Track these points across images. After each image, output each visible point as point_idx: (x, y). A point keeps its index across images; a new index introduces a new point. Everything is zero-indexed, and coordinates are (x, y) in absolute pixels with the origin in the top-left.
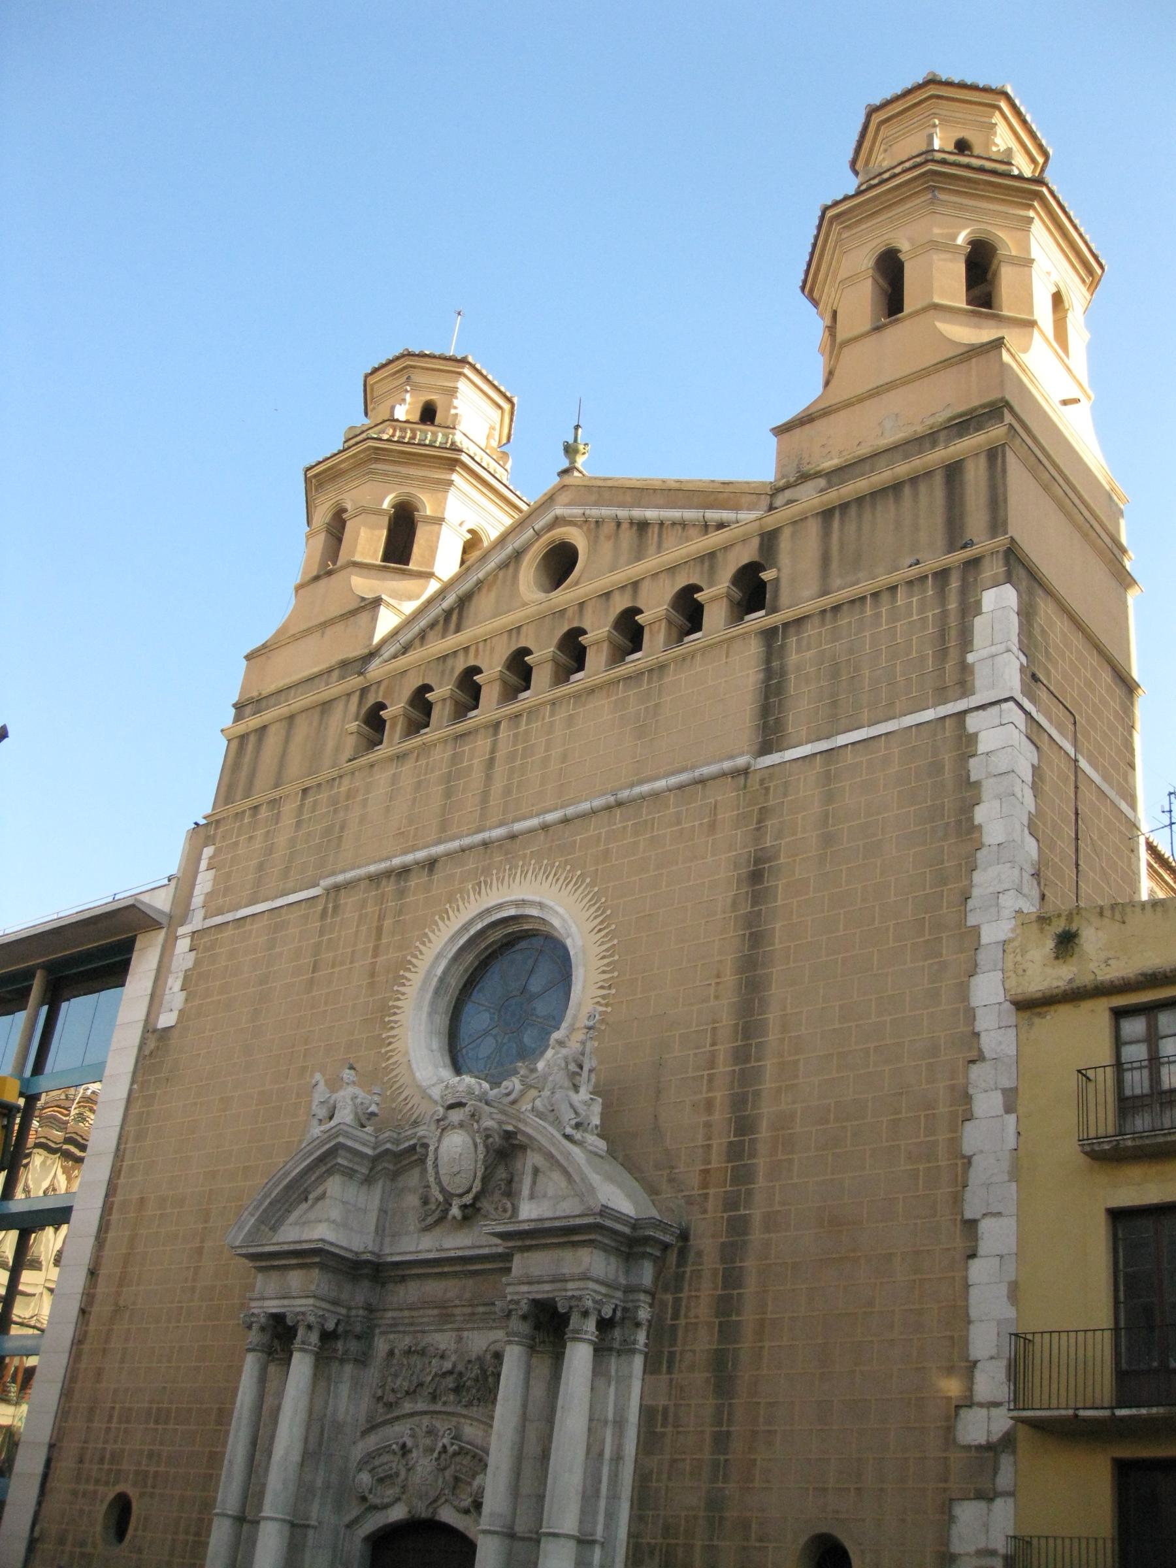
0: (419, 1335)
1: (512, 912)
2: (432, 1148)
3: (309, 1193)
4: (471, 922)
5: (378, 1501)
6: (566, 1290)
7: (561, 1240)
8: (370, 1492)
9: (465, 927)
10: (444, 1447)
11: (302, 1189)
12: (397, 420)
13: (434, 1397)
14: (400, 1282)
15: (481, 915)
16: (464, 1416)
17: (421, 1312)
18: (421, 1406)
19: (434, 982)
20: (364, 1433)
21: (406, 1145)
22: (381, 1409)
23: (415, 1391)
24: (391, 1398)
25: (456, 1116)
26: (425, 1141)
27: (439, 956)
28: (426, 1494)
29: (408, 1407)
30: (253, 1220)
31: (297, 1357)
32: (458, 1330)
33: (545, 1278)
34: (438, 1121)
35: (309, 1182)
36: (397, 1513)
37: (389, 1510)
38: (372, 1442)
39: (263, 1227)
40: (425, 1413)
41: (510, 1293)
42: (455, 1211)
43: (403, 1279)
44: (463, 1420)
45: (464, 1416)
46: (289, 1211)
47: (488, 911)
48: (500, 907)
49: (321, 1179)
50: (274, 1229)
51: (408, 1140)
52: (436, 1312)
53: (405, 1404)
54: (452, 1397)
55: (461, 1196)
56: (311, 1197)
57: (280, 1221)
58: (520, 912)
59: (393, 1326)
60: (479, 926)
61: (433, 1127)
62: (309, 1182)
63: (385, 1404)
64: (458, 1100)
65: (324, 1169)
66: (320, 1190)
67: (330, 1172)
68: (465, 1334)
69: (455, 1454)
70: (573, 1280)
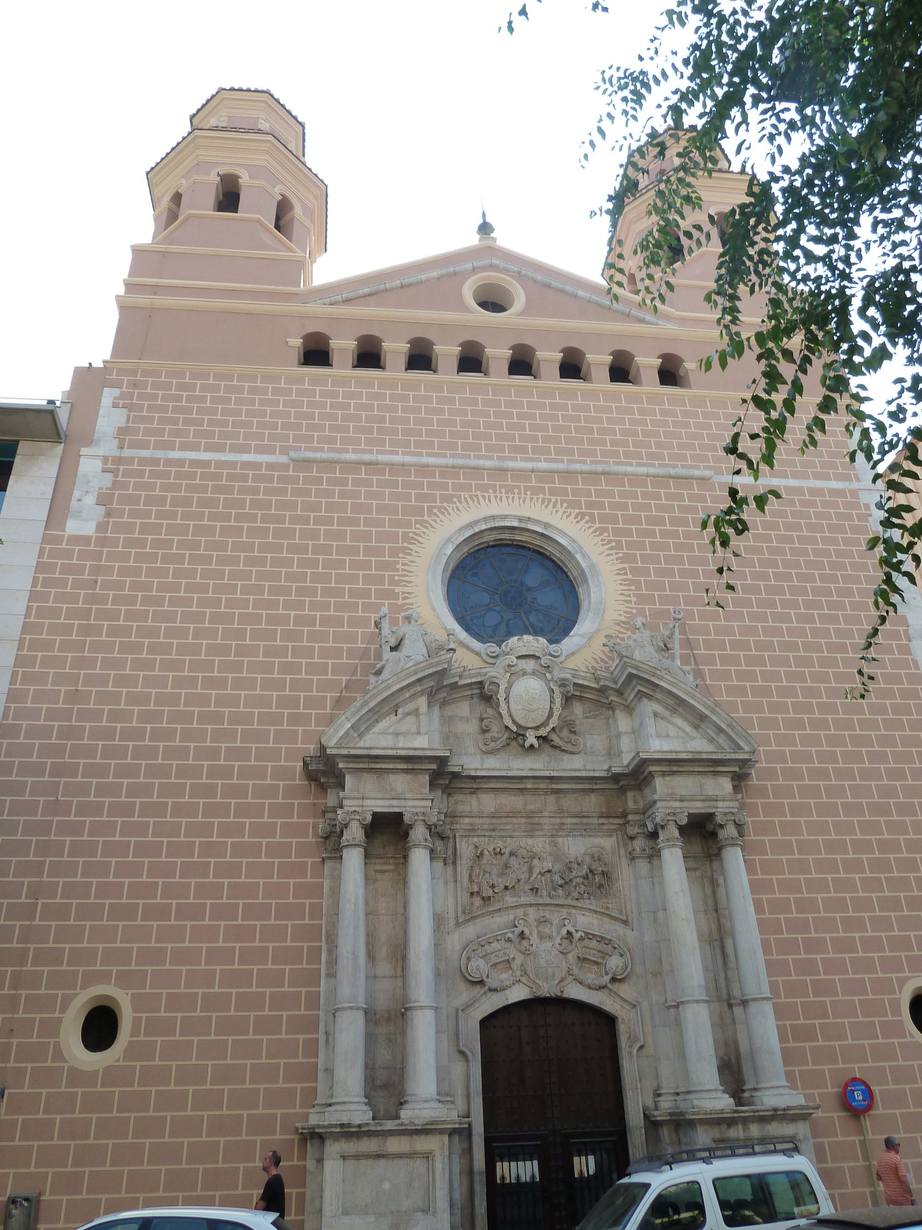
0: (509, 840)
1: (516, 524)
2: (502, 687)
3: (398, 707)
4: (476, 522)
5: (495, 984)
6: (717, 808)
7: (706, 770)
8: (488, 977)
9: (471, 525)
10: (569, 932)
11: (394, 703)
12: (732, 172)
13: (536, 891)
14: (471, 793)
15: (486, 519)
16: (574, 907)
17: (504, 820)
18: (524, 899)
19: (445, 559)
20: (458, 924)
21: (469, 681)
22: (477, 901)
23: (513, 887)
24: (488, 892)
25: (530, 665)
26: (496, 681)
27: (449, 540)
28: (553, 975)
29: (510, 900)
30: (349, 725)
31: (666, 854)
32: (552, 836)
33: (697, 798)
34: (510, 666)
35: (402, 698)
36: (517, 994)
37: (507, 992)
38: (470, 931)
39: (352, 732)
40: (531, 905)
41: (662, 808)
42: (531, 740)
43: (475, 791)
44: (574, 911)
45: (574, 907)
46: (377, 721)
47: (493, 518)
48: (505, 517)
49: (414, 696)
50: (361, 736)
51: (471, 678)
52: (523, 820)
53: (507, 898)
54: (560, 892)
55: (537, 728)
56: (400, 711)
57: (367, 729)
58: (523, 525)
59: (472, 830)
60: (484, 527)
61: (502, 671)
62: (402, 698)
63: (483, 898)
64: (532, 653)
65: (419, 689)
66: (411, 706)
67: (422, 692)
68: (560, 839)
69: (581, 939)
70: (723, 801)
